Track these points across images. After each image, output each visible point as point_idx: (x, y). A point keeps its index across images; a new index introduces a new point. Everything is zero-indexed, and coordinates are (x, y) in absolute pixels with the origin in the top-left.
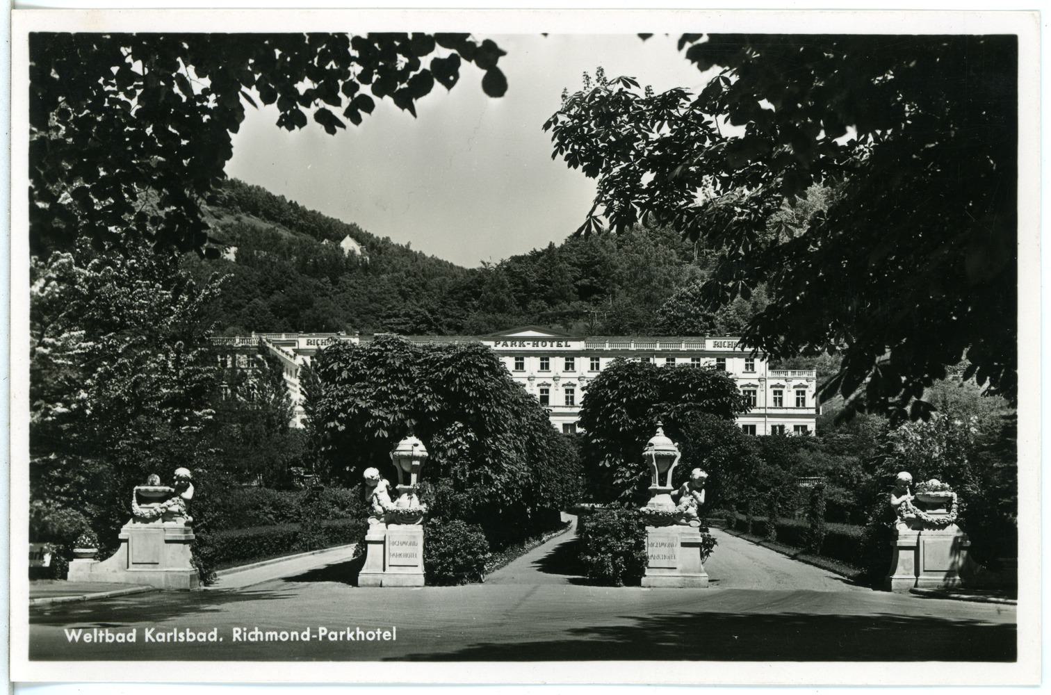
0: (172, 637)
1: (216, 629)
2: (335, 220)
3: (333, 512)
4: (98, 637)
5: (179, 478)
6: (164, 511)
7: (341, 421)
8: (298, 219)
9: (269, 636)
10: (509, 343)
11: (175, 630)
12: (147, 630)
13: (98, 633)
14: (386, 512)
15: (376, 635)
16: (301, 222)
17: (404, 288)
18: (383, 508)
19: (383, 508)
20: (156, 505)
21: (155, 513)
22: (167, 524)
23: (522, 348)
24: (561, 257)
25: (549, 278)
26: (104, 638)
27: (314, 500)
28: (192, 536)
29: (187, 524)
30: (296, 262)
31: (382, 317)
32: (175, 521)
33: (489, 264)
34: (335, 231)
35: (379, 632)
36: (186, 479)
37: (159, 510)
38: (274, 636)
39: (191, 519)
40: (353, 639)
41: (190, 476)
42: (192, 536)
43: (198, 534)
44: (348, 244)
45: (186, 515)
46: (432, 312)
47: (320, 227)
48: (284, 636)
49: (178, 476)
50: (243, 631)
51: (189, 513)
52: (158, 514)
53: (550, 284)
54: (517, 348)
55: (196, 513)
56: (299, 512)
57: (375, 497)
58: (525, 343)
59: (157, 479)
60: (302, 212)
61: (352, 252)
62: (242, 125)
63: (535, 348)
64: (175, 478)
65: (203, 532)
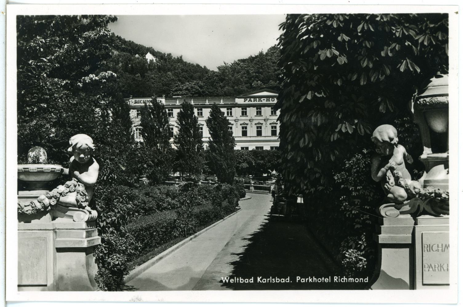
0: (269, 281)
1: (253, 278)
2: (141, 45)
3: (167, 201)
4: (237, 280)
5: (78, 150)
6: (53, 202)
7: (340, 46)
8: (122, 45)
9: (350, 280)
10: (252, 99)
11: (271, 277)
12: (258, 278)
13: (237, 279)
14: (411, 195)
15: (322, 280)
16: (123, 46)
17: (181, 78)
18: (407, 190)
19: (407, 190)
20: (42, 194)
21: (39, 206)
22: (61, 222)
23: (260, 102)
24: (267, 59)
25: (261, 70)
26: (239, 281)
27: (188, 190)
28: (97, 239)
29: (90, 222)
30: (122, 66)
31: (173, 91)
32: (71, 217)
33: (227, 64)
34: (142, 50)
35: (323, 279)
36: (87, 151)
37: (47, 202)
38: (352, 280)
39: (95, 213)
40: (312, 281)
41: (92, 146)
42: (97, 239)
43: (106, 236)
44: (149, 57)
45: (88, 208)
46: (201, 87)
47: (134, 49)
48: (246, 281)
49: (74, 147)
50: (338, 278)
51: (92, 205)
52: (45, 207)
53: (261, 73)
54: (257, 102)
55: (100, 204)
56: (145, 202)
57: (389, 174)
58: (262, 99)
59: (42, 154)
60: (124, 42)
61: (151, 61)
62: (54, 221)
63: (268, 102)
64: (70, 149)
65: (112, 233)
